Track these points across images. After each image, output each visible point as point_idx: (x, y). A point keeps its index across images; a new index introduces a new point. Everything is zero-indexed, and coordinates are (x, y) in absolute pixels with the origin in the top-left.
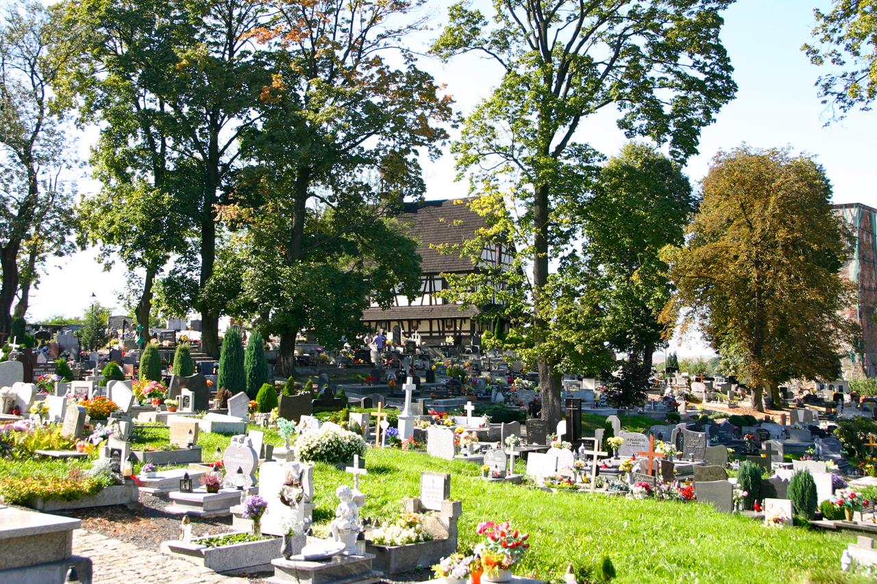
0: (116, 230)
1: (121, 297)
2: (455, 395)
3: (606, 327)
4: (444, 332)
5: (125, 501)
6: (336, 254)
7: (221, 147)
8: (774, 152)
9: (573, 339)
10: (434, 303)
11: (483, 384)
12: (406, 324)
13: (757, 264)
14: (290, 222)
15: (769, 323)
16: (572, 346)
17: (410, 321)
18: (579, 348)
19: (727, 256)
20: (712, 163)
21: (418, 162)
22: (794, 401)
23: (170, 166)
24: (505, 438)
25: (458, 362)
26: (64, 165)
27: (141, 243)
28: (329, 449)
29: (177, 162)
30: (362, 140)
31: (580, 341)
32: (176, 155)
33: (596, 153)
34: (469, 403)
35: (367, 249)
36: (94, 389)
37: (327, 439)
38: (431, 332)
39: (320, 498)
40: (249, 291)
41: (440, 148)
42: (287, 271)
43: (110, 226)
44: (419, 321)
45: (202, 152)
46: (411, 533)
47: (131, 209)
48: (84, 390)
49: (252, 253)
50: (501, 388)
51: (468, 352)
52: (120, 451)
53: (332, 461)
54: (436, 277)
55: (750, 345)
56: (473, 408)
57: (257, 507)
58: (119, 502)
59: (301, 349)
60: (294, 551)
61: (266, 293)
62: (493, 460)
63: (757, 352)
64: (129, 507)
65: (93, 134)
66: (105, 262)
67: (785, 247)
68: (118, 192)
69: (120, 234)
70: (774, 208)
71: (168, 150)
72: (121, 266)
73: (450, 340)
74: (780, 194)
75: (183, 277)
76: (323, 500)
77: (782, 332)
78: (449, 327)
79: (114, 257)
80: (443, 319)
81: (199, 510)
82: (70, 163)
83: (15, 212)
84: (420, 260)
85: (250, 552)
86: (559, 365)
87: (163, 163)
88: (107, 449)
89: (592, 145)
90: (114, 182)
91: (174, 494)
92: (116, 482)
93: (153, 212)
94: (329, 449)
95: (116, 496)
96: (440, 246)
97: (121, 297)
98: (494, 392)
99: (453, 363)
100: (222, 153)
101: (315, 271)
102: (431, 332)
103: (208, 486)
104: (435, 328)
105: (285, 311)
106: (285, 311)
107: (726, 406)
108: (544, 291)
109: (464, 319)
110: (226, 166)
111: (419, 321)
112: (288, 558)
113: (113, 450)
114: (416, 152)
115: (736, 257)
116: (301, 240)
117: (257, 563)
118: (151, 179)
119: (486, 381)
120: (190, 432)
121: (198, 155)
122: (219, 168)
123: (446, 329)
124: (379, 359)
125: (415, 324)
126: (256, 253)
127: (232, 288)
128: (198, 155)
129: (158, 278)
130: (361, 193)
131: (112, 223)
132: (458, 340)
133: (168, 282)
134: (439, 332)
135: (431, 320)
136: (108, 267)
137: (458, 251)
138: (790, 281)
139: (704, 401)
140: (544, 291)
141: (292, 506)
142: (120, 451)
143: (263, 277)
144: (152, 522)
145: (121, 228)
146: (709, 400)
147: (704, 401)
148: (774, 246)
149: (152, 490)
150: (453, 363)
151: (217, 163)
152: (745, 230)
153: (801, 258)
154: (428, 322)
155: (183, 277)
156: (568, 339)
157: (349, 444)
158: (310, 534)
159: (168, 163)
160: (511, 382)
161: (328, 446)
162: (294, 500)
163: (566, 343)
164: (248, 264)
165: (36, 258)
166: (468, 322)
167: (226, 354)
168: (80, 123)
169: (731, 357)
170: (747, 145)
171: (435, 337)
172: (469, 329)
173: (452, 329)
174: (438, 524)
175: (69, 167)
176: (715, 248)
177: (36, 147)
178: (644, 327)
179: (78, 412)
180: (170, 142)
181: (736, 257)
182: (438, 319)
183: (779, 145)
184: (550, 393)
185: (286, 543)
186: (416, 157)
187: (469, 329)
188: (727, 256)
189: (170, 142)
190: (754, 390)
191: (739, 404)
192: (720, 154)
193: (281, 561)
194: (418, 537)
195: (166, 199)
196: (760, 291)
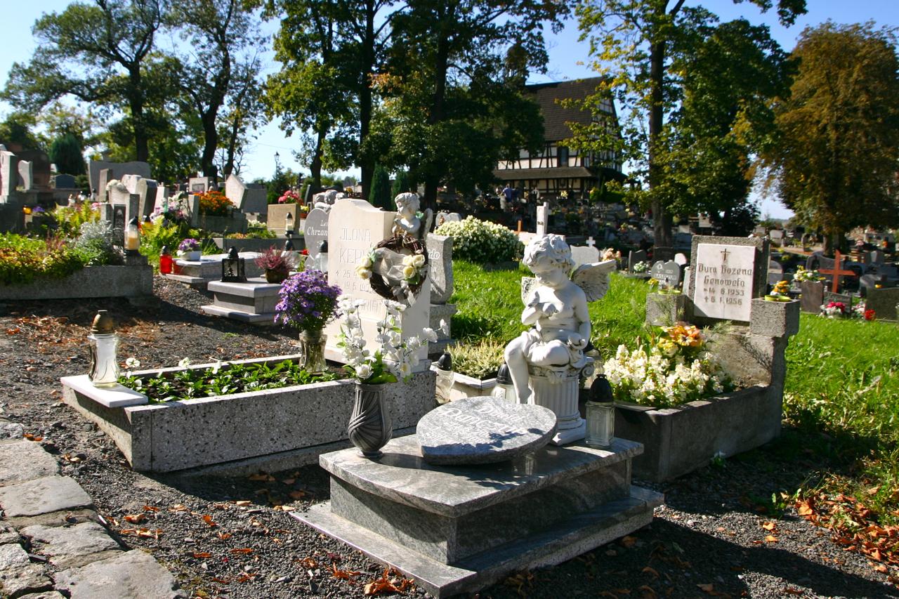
0: (291, 98)
1: (299, 156)
2: (575, 234)
3: (716, 171)
4: (558, 189)
5: (127, 291)
6: (472, 116)
7: (375, 32)
8: (857, 27)
9: (687, 181)
10: (550, 166)
11: (596, 227)
12: (527, 183)
13: (836, 127)
14: (433, 88)
15: (846, 179)
16: (685, 187)
17: (531, 181)
18: (691, 191)
19: (810, 120)
20: (801, 38)
21: (542, 35)
22: (856, 247)
23: (336, 48)
24: (632, 265)
25: (573, 210)
26: (248, 42)
27: (312, 109)
28: (473, 245)
29: (342, 44)
30: (494, 17)
31: (693, 184)
32: (340, 39)
33: (708, 15)
34: (591, 238)
35: (499, 112)
36: (209, 185)
37: (471, 232)
38: (548, 189)
39: (464, 300)
40: (398, 145)
41: (562, 21)
42: (430, 128)
43: (287, 96)
44: (538, 180)
45: (361, 35)
46: (688, 374)
47: (304, 84)
48: (201, 187)
49: (401, 113)
50: (611, 230)
51: (580, 205)
52: (123, 208)
53: (478, 260)
54: (553, 144)
55: (825, 199)
56: (594, 242)
57: (309, 298)
58: (115, 292)
59: (443, 198)
60: (389, 426)
61: (413, 147)
62: (663, 272)
63: (831, 204)
64: (132, 302)
65: (274, 26)
66: (287, 129)
67: (865, 112)
68: (294, 70)
69: (295, 102)
70: (859, 76)
71: (334, 34)
72: (298, 132)
73: (564, 194)
74: (866, 62)
75: (346, 138)
76: (469, 304)
77: (854, 188)
78: (563, 185)
79: (293, 124)
80: (558, 180)
81: (250, 311)
82: (252, 40)
83: (213, 84)
84: (543, 121)
85: (282, 415)
86: (671, 206)
87: (330, 46)
88: (109, 206)
89: (704, 7)
90: (291, 62)
91: (216, 284)
92: (111, 259)
93: (321, 80)
94: (473, 245)
95: (115, 283)
96: (564, 101)
97: (299, 156)
98: (607, 233)
99: (569, 211)
100: (376, 36)
101: (453, 127)
102: (548, 189)
103: (268, 271)
104: (551, 186)
105: (429, 162)
106: (429, 162)
107: (802, 250)
108: (660, 138)
109: (574, 179)
110: (380, 47)
111: (538, 180)
112: (373, 454)
113: (117, 207)
114: (541, 27)
115: (818, 122)
116: (444, 104)
117: (304, 441)
118: (319, 58)
119: (599, 225)
120: (290, 216)
121: (358, 38)
122: (375, 48)
123: (560, 187)
124: (507, 207)
125: (534, 183)
126: (404, 113)
127: (384, 143)
128: (358, 38)
129: (327, 137)
130: (494, 64)
131: (289, 93)
132: (571, 194)
133: (332, 142)
134: (554, 189)
135: (547, 180)
136: (289, 133)
137: (580, 105)
138: (867, 142)
139: (782, 246)
140: (660, 138)
141: (402, 297)
142: (123, 208)
143: (409, 134)
144: (172, 329)
145: (296, 96)
146: (786, 245)
147: (782, 246)
148: (856, 110)
149: (189, 279)
150: (569, 211)
151: (373, 43)
152: (828, 97)
153: (880, 120)
154: (545, 182)
155: (346, 138)
156: (683, 182)
157: (500, 240)
158: (446, 365)
159: (334, 45)
160: (619, 227)
161: (472, 241)
162: (404, 284)
163: (679, 185)
164: (397, 123)
165: (238, 130)
166: (579, 181)
167: (375, 189)
168: (265, 16)
169: (805, 209)
170: (832, 22)
171: (551, 194)
172: (579, 187)
173: (565, 187)
174: (742, 352)
175: (251, 43)
176: (800, 113)
177: (228, 31)
178: (727, 186)
179: (146, 186)
180: (335, 27)
181: (818, 122)
182: (553, 179)
183: (861, 20)
184: (662, 230)
185: (365, 407)
186: (541, 31)
187: (579, 187)
188: (810, 120)
189: (335, 27)
190: (826, 236)
191: (812, 249)
192: (807, 30)
193: (345, 461)
194: (709, 384)
195: (331, 72)
196: (838, 151)
